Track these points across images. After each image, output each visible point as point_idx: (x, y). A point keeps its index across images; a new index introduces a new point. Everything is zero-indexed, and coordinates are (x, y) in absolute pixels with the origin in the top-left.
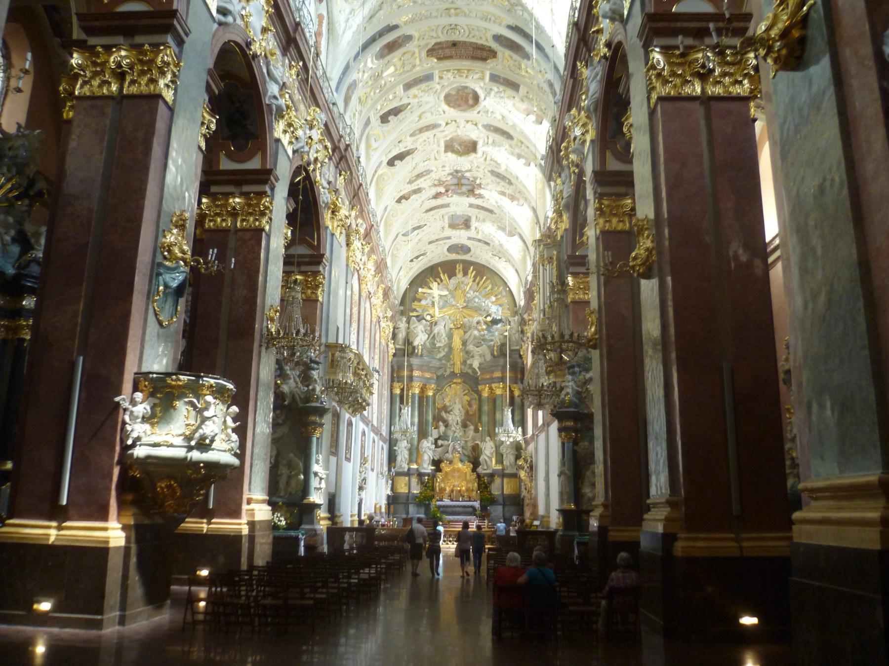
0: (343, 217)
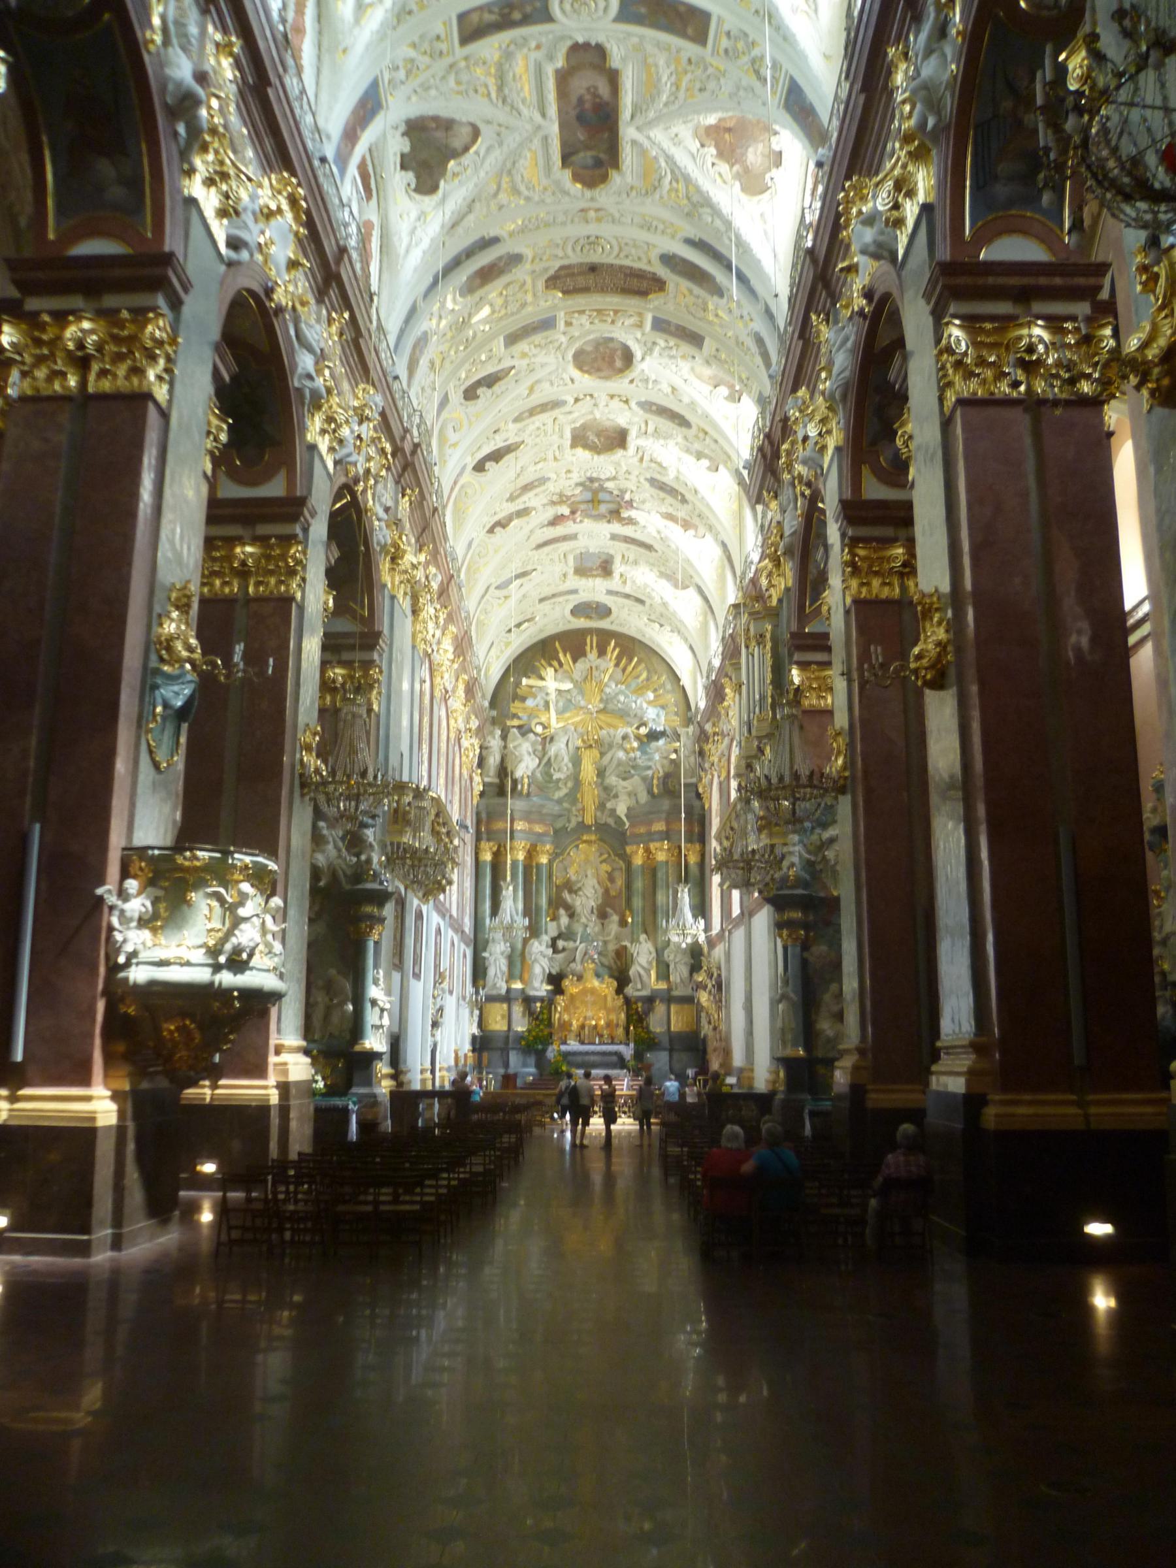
0: (409, 566)
